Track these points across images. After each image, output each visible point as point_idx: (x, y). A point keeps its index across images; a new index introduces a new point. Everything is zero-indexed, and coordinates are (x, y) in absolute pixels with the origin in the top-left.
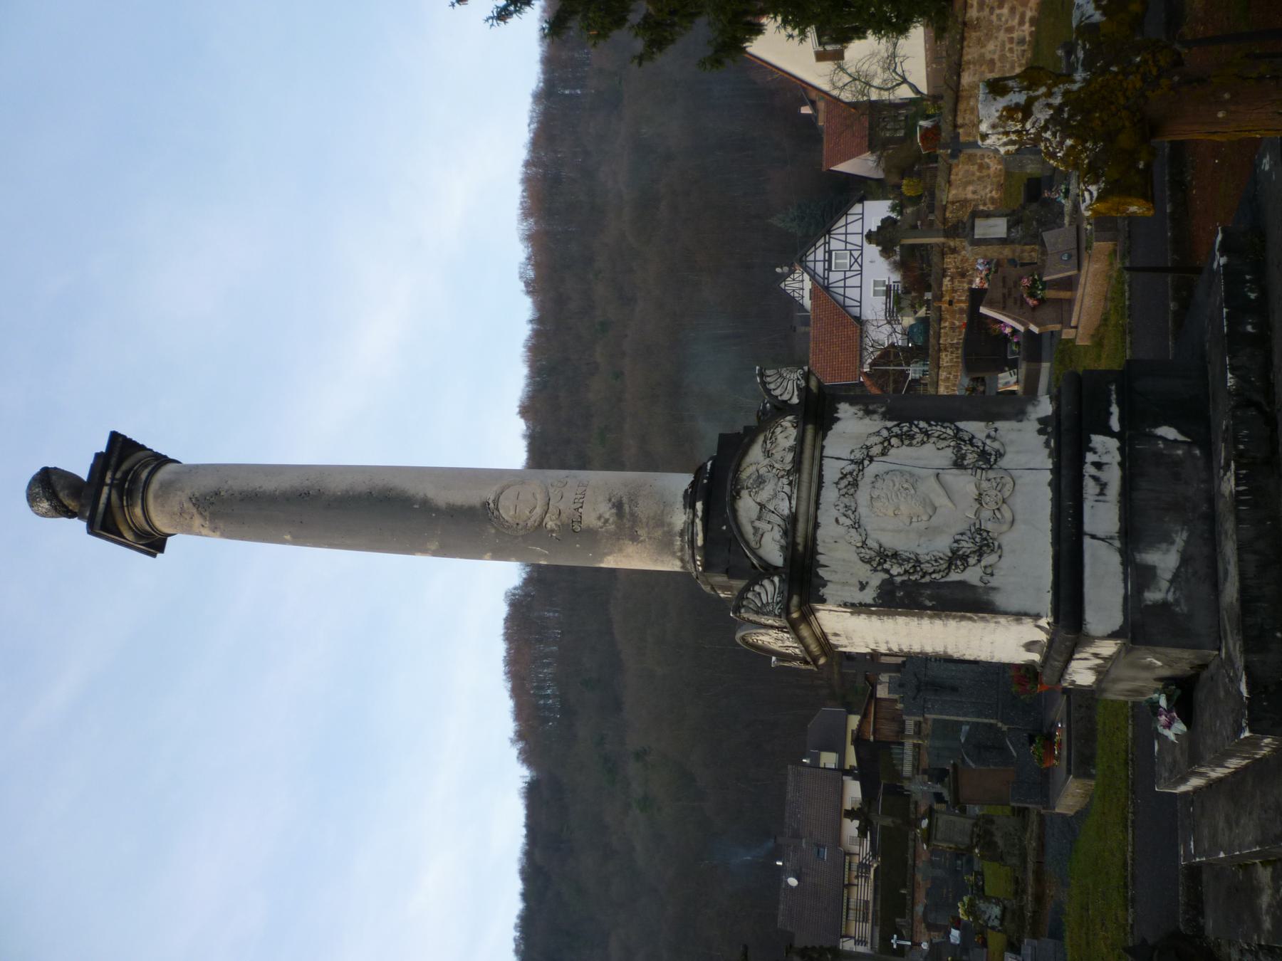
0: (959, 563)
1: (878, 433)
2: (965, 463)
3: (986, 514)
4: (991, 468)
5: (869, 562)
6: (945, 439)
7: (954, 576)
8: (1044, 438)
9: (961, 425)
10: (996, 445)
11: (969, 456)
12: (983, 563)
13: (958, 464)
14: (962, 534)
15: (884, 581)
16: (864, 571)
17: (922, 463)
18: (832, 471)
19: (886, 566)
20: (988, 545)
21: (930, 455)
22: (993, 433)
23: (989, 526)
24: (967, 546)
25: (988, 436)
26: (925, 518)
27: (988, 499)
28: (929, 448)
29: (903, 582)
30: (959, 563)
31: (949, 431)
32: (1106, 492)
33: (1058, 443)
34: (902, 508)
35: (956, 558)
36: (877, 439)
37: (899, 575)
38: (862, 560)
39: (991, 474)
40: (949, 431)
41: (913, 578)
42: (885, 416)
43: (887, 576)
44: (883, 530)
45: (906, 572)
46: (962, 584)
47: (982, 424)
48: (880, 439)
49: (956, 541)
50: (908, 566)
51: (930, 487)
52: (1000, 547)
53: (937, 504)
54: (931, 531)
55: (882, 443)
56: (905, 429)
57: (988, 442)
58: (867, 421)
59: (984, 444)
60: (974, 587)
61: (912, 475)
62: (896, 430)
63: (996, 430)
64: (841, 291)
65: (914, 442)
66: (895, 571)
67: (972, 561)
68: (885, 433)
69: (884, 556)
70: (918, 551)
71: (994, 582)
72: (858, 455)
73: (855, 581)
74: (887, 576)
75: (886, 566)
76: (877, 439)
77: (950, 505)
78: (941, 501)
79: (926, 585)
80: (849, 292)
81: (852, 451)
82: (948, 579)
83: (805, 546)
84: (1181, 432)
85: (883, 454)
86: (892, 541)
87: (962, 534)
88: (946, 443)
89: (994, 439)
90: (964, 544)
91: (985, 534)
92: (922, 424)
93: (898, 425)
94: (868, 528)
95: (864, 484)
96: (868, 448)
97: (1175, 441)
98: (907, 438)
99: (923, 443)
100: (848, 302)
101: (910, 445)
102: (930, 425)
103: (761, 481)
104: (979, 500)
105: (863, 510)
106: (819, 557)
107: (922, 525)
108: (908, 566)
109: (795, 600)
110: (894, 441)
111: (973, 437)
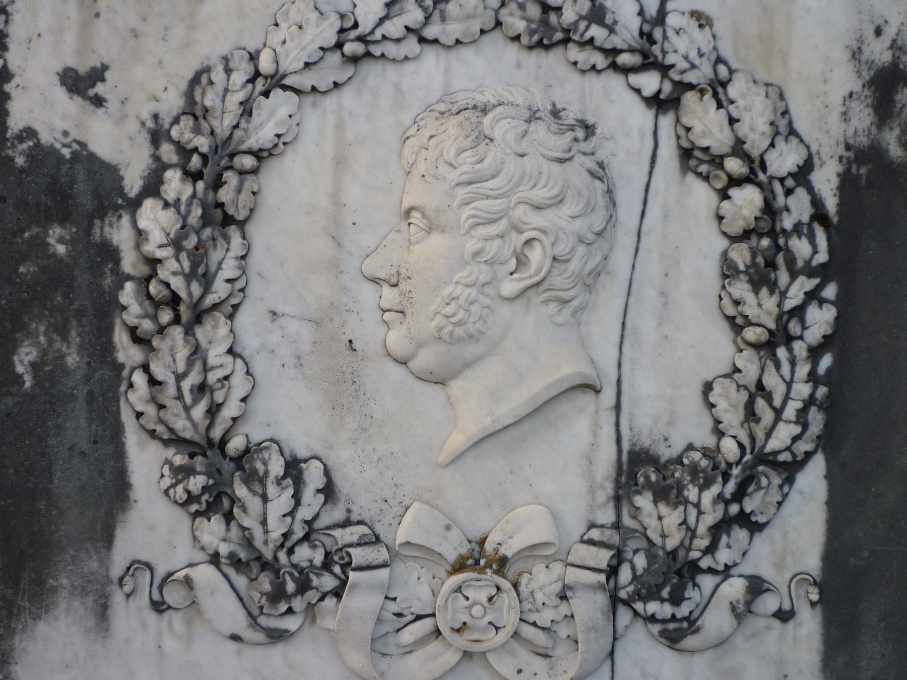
0: (196, 483)
1: (784, 129)
2: (644, 501)
3: (416, 587)
4: (615, 601)
5: (194, 111)
6: (751, 414)
7: (145, 462)
9: (813, 479)
10: (716, 620)
11: (673, 517)
12: (205, 574)
13: (639, 471)
14: (329, 491)
15: (104, 175)
16: (149, 84)
17: (645, 322)
19: (174, 184)
20: (278, 595)
21: (680, 347)
22: (769, 603)
23: (362, 600)
24: (270, 514)
25: (757, 587)
26: (396, 339)
27: (479, 594)
28: (716, 348)
29: (111, 253)
30: (196, 483)
31: (784, 434)
32: (702, 508)
34: (436, 241)
35: (218, 470)
36: (755, 127)
37: (140, 235)
38: (199, 78)
39: (589, 606)
40: (784, 434)
41: (128, 294)
42: (863, 160)
43: (133, 183)
44: (340, 162)
46: (117, 491)
47: (812, 562)
48: (756, 143)
49: (294, 468)
50: (171, 272)
51: (536, 354)
52: (277, 636)
53: (456, 387)
54: (340, 366)
55: (739, 149)
56: (801, 247)
57: (735, 588)
58: (846, 79)
59: (726, 572)
60: (106, 538)
61: (590, 282)
62: (798, 208)
63: (784, 616)
65: (741, 289)
66: (155, 219)
67: (212, 530)
68: (785, 159)
69: (217, 171)
71: (129, 614)
72: (683, 45)
73: (104, 47)
74: (133, 183)
75: (174, 184)
76: (755, 127)
77: (457, 441)
78: (476, 405)
79: (101, 350)
81: (702, 19)
82: (132, 438)
84: (839, 212)
85: (686, 154)
86: (288, 206)
87: (329, 491)
88: (732, 419)
89: (742, 612)
90: (281, 501)
91: (328, 582)
92: (820, 320)
93: (820, 216)
94: (347, 95)
95: (554, 77)
96: (717, 89)
98: (761, 253)
99: (737, 324)
101: (729, 271)
102: (815, 353)
104: (479, 559)
105: (428, 73)
107: (367, 330)
108: (171, 272)
110: (747, 201)
111: (755, 528)
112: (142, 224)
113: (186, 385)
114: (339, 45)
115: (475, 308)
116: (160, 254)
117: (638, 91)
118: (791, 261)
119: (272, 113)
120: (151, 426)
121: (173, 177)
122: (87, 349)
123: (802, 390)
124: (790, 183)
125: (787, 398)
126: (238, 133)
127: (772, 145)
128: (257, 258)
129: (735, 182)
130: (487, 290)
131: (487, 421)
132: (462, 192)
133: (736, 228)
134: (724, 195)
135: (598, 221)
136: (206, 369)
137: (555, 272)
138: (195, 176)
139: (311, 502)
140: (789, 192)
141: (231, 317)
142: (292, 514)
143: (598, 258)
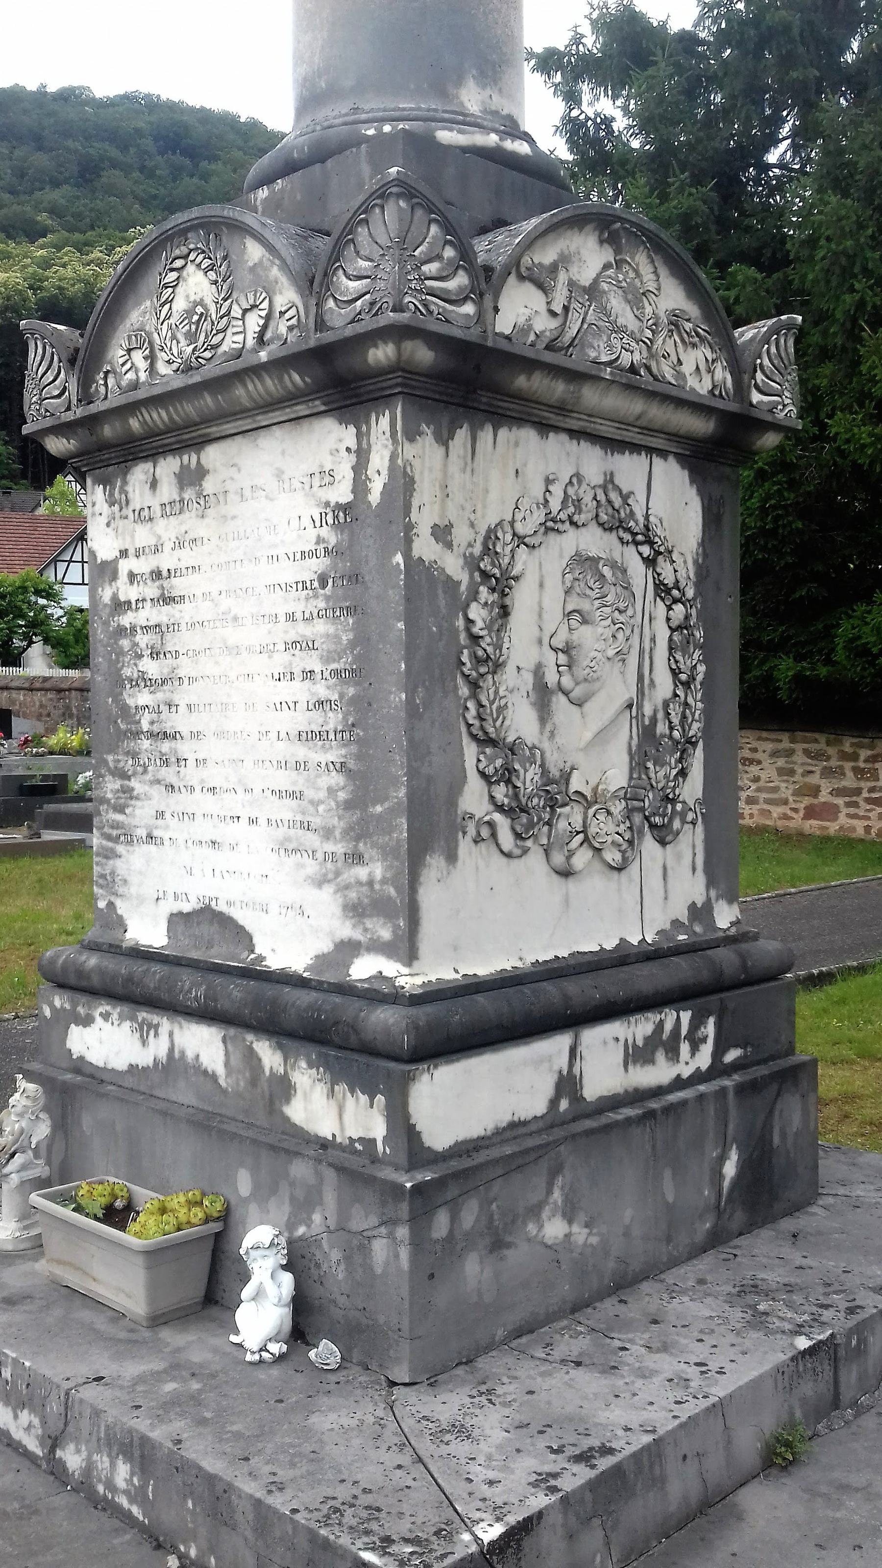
8: (684, 918)
12: (497, 817)
18: (630, 470)
30: (499, 762)
33: (679, 951)
37: (470, 622)
38: (491, 536)
45: (475, 639)
47: (700, 795)
53: (587, 706)
64: (77, 557)
67: (501, 792)
70: (510, 668)
80: (75, 568)
83: (519, 397)
97: (721, 1176)
100: (61, 567)
103: (636, 298)
106: (488, 430)
109: (423, 355)
112: (471, 616)
113: (494, 707)
116: (481, 633)
117: (641, 554)
120: (475, 732)
121: (483, 590)
122: (790, 697)
129: (676, 601)
131: (600, 723)
132: (597, 602)
133: (674, 624)
134: (669, 608)
138: (493, 590)
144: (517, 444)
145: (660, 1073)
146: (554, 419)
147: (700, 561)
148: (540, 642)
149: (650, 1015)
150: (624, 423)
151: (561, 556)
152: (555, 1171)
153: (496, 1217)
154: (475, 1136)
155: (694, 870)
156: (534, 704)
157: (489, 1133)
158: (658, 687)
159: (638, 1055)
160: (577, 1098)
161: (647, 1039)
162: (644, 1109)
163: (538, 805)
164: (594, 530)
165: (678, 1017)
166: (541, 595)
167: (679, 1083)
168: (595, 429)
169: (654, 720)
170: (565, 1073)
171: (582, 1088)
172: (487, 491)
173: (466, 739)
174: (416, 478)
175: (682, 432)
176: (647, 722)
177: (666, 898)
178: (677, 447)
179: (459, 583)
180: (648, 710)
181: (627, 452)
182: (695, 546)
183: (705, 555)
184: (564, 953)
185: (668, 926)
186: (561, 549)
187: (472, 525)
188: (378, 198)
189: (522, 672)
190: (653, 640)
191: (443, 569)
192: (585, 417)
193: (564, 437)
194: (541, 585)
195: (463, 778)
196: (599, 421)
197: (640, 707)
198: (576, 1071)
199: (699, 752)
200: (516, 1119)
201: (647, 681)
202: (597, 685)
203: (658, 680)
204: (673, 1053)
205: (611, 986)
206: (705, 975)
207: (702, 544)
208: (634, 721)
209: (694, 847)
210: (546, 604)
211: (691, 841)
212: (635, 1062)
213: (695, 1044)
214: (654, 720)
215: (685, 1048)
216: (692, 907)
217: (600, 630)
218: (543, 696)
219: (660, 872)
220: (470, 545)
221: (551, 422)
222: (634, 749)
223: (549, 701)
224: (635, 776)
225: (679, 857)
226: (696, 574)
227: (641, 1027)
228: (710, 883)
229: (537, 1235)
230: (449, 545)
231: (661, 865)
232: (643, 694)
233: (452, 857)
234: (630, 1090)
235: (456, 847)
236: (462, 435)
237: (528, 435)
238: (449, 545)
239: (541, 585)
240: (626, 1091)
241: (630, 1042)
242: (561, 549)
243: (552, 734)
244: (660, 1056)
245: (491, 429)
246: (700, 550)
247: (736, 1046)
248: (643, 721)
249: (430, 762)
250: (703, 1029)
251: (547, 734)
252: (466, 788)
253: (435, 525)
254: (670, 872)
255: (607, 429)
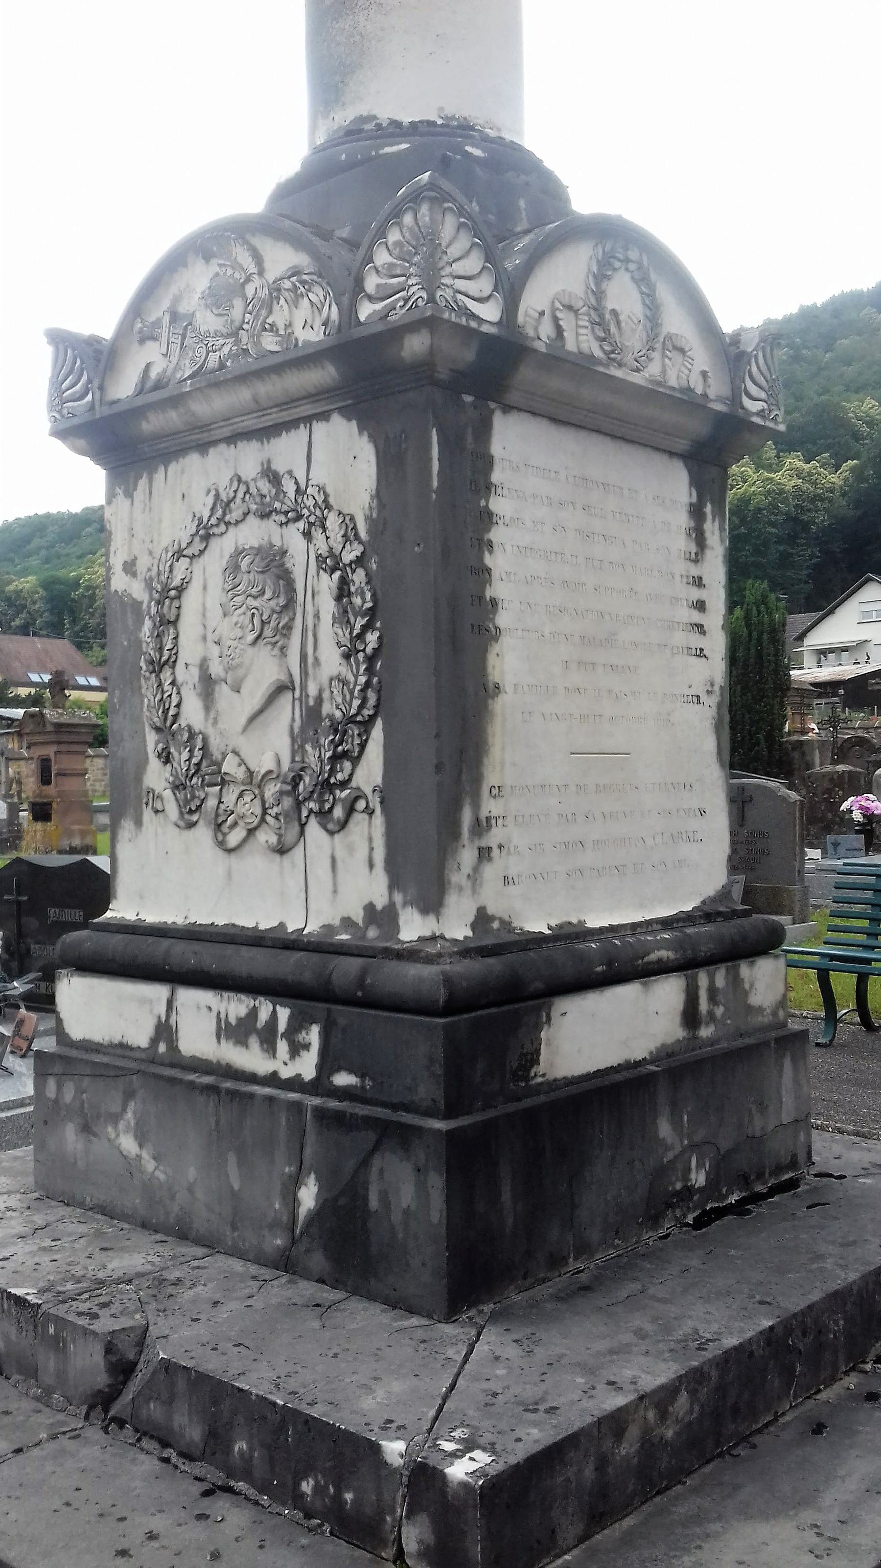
8: (358, 916)
18: (287, 451)
47: (379, 780)
51: (264, 669)
114: (197, 532)
115: (237, 651)
118: (353, 608)
119: (180, 569)
123: (362, 679)
124: (353, 566)
125: (355, 684)
126: (169, 580)
127: (344, 547)
128: (182, 640)
130: (241, 641)
135: (282, 601)
136: (163, 692)
137: (266, 628)
139: (198, 754)
140: (354, 571)
141: (173, 667)
142: (189, 760)
143: (286, 619)
144: (183, 472)
145: (251, 1059)
146: (205, 437)
147: (374, 515)
148: (204, 638)
149: (243, 997)
150: (260, 409)
151: (222, 556)
152: (129, 1095)
153: (86, 1105)
154: (96, 1041)
155: (371, 866)
156: (199, 695)
157: (105, 1043)
158: (323, 664)
159: (236, 1032)
160: (173, 1047)
161: (240, 1020)
162: (222, 1086)
163: (197, 784)
164: (253, 521)
165: (274, 1012)
166: (204, 596)
167: (273, 1079)
168: (243, 428)
169: (319, 700)
170: (163, 1020)
171: (177, 1040)
172: (160, 521)
173: (147, 729)
174: (113, 531)
175: (312, 390)
176: (311, 702)
177: (335, 891)
178: (344, 400)
179: (142, 603)
180: (312, 690)
181: (284, 433)
182: (367, 499)
183: (381, 506)
184: (220, 921)
185: (337, 922)
186: (222, 549)
187: (151, 553)
188: (410, 201)
189: (189, 667)
190: (317, 616)
191: (130, 595)
192: (222, 424)
193: (223, 447)
194: (205, 588)
195: (146, 760)
196: (236, 420)
197: (304, 687)
198: (172, 1021)
199: (377, 732)
200: (125, 1041)
201: (310, 660)
202: (240, 672)
203: (323, 658)
204: (269, 1047)
205: (208, 958)
206: (307, 977)
207: (378, 495)
208: (297, 703)
209: (370, 840)
210: (209, 605)
211: (368, 833)
212: (228, 1038)
213: (296, 1049)
214: (319, 700)
215: (282, 1047)
216: (370, 908)
217: (235, 619)
218: (208, 685)
219: (327, 863)
220: (149, 570)
221: (207, 440)
222: (296, 730)
223: (213, 690)
224: (297, 759)
225: (351, 849)
226: (369, 532)
227: (236, 1006)
228: (394, 884)
229: (114, 1140)
230: (134, 575)
231: (329, 853)
232: (307, 674)
233: (139, 823)
234: (223, 1063)
235: (141, 814)
236: (143, 483)
237: (193, 459)
238: (134, 575)
239: (205, 588)
240: (218, 1062)
241: (223, 1016)
242: (222, 549)
243: (215, 721)
244: (254, 1042)
245: (163, 468)
246: (374, 505)
247: (351, 1071)
248: (307, 703)
249: (123, 747)
250: (304, 1033)
251: (211, 721)
252: (148, 768)
253: (126, 562)
254: (339, 864)
255: (251, 423)
